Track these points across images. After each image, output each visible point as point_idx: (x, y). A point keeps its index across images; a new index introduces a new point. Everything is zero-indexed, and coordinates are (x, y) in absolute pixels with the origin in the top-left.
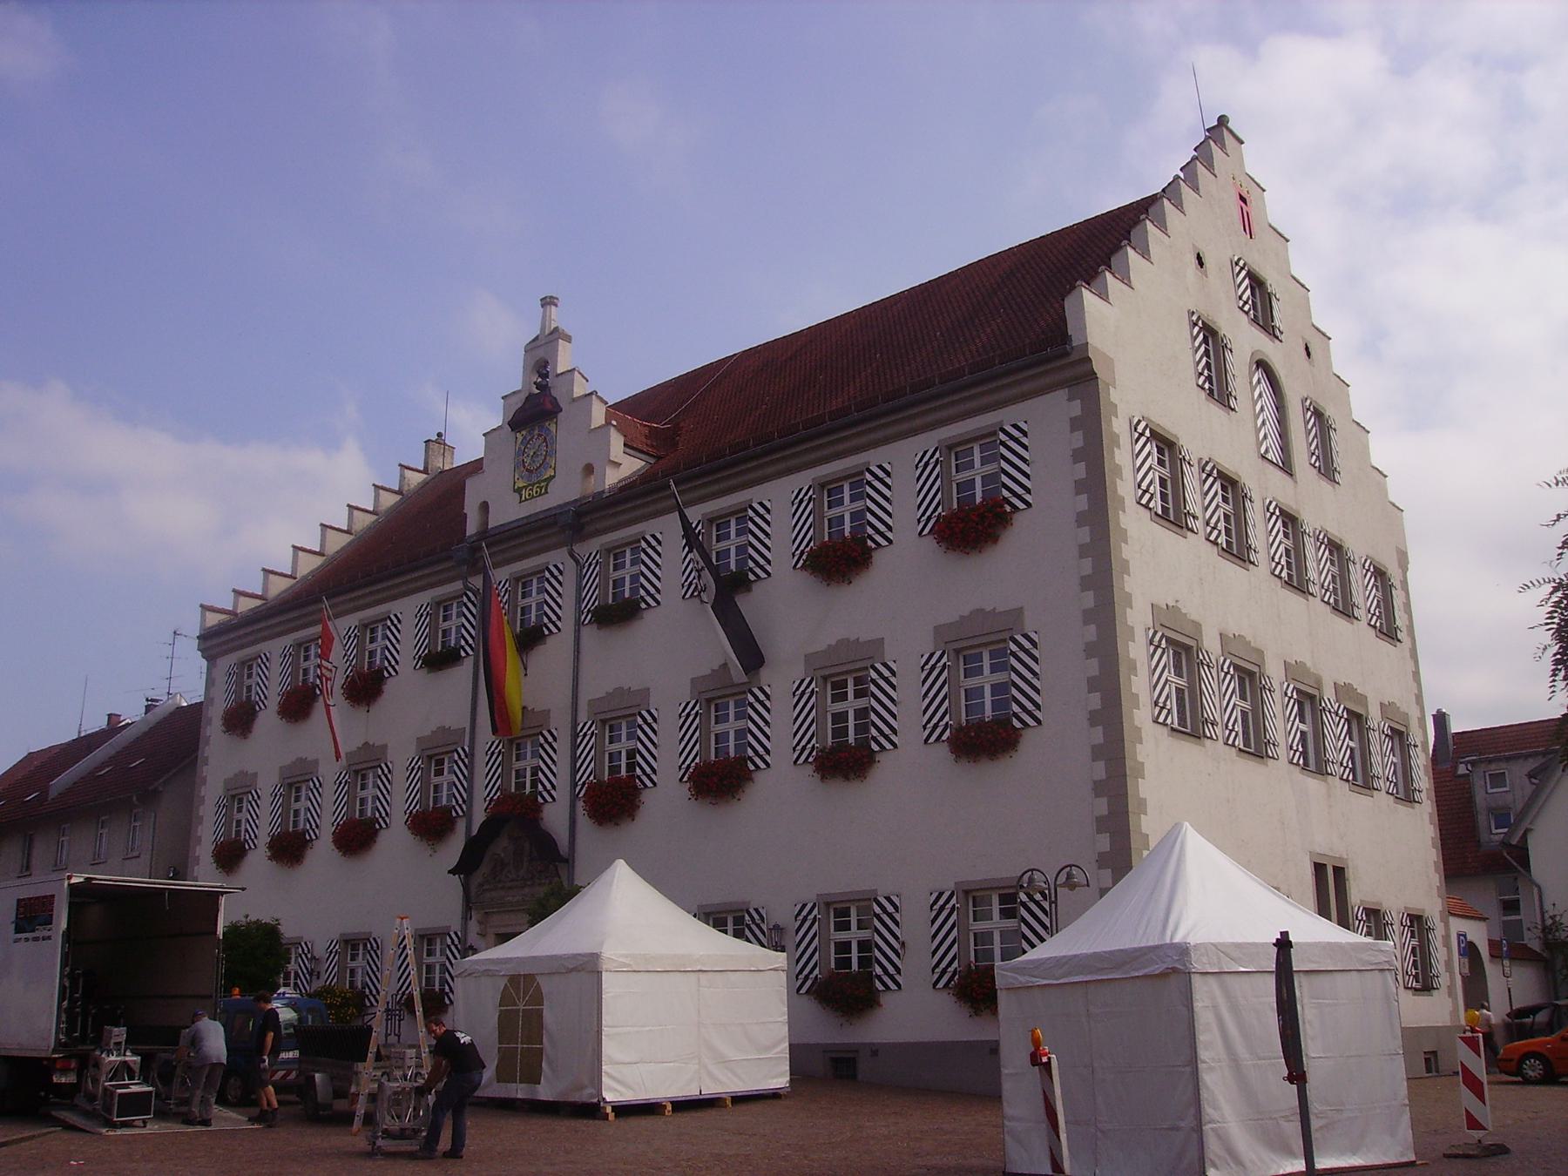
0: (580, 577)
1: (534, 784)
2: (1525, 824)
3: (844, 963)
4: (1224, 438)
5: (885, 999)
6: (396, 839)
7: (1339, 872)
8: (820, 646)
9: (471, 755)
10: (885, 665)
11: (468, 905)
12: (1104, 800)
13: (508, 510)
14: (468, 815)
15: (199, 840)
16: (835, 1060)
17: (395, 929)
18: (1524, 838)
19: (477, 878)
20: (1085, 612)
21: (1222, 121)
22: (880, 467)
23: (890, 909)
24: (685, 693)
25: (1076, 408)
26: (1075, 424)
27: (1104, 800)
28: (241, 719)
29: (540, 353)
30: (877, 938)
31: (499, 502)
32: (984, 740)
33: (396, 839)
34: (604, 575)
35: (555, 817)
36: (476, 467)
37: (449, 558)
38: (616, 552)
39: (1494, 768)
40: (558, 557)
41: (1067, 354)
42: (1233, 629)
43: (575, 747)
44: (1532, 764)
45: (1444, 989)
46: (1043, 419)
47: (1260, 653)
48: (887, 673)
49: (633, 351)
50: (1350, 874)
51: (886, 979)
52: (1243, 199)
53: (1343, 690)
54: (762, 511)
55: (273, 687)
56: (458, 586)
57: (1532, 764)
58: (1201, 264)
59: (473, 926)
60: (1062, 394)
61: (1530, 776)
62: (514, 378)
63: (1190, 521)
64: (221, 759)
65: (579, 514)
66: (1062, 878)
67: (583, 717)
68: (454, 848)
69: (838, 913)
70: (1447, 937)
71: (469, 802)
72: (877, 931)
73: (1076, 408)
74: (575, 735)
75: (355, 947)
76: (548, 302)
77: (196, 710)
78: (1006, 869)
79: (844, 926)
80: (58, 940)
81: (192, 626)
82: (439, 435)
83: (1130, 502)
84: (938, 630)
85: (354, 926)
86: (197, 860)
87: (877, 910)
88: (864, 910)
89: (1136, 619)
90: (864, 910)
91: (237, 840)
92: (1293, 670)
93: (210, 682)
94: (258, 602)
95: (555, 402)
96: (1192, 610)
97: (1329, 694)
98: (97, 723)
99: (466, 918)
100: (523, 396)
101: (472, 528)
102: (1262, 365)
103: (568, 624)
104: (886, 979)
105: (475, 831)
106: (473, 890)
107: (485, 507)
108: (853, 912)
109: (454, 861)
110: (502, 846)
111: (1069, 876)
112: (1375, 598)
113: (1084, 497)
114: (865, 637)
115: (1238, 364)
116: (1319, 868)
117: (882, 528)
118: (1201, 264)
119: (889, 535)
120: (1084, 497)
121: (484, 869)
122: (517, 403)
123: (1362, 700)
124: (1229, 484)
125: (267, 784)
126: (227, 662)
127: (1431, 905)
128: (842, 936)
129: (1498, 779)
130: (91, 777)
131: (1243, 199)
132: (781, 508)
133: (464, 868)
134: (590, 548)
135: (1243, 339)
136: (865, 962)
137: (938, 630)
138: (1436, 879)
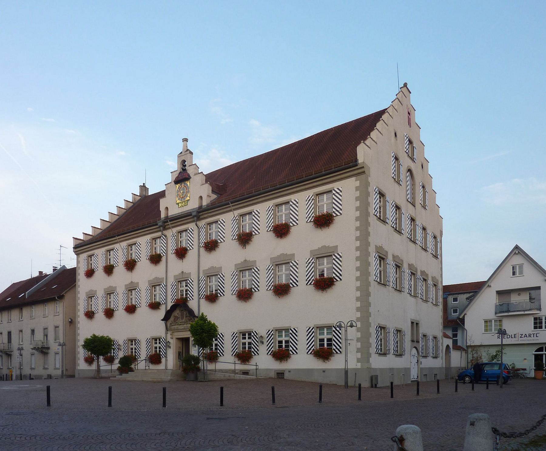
0: (199, 232)
1: (186, 294)
2: (466, 311)
3: (280, 347)
4: (397, 194)
5: (293, 356)
6: (143, 310)
7: (417, 324)
8: (151, 279)
9: (166, 286)
10: (295, 262)
11: (167, 329)
12: (359, 242)
13: (174, 211)
14: (166, 304)
15: (79, 310)
16: (278, 373)
17: (143, 336)
18: (464, 316)
19: (169, 323)
20: (358, 349)
21: (405, 85)
22: (295, 200)
23: (295, 332)
24: (233, 268)
25: (358, 183)
26: (357, 189)
27: (359, 242)
28: (90, 273)
29: (183, 158)
30: (291, 340)
31: (170, 206)
32: (324, 284)
33: (143, 310)
34: (206, 232)
35: (193, 304)
36: (162, 194)
37: (157, 225)
38: (210, 224)
39: (455, 296)
40: (192, 226)
41: (356, 165)
42: (396, 254)
43: (199, 284)
44: (468, 295)
45: (440, 358)
46: (347, 188)
47: (402, 261)
48: (295, 264)
49: (211, 159)
50: (420, 325)
51: (293, 351)
52: (409, 113)
53: (423, 273)
54: (257, 213)
55: (99, 263)
56: (159, 234)
57: (468, 295)
58: (395, 134)
59: (169, 336)
60: (354, 179)
61: (467, 299)
62: (174, 166)
63: (387, 221)
64: (84, 285)
65: (199, 212)
66: (349, 324)
67: (201, 275)
68: (161, 313)
69: (243, 335)
70: (442, 343)
71: (166, 299)
72: (334, 336)
73: (358, 183)
74: (199, 280)
75: (156, 340)
76: (185, 140)
77: (73, 271)
78: (333, 321)
79: (245, 338)
80: (372, 325)
81: (71, 244)
82: (144, 184)
83: (371, 214)
84: (311, 252)
85: (131, 336)
86: (79, 316)
87: (291, 332)
88: (250, 334)
89: (372, 249)
90: (250, 334)
91: (110, 309)
92: (410, 266)
93: (78, 262)
94: (91, 237)
95: (189, 175)
96: (386, 248)
97: (419, 273)
98: (36, 274)
99: (166, 333)
100: (178, 172)
101: (163, 215)
102: (409, 170)
103: (196, 247)
104: (293, 351)
105: (169, 308)
106: (168, 325)
107: (167, 208)
108: (247, 334)
109: (162, 317)
110: (177, 313)
111: (352, 324)
112: (431, 243)
113: (358, 212)
114: (289, 253)
115: (403, 170)
116: (412, 323)
117: (295, 220)
118: (395, 134)
119: (297, 222)
120: (358, 212)
121: (172, 319)
122: (176, 175)
123: (427, 275)
124: (398, 208)
125: (100, 293)
126: (84, 256)
127: (439, 335)
128: (244, 341)
129: (455, 300)
130: (38, 291)
131: (409, 113)
132: (263, 213)
133: (166, 319)
134: (202, 223)
135: (406, 162)
136: (287, 346)
137: (311, 252)
138: (441, 327)
